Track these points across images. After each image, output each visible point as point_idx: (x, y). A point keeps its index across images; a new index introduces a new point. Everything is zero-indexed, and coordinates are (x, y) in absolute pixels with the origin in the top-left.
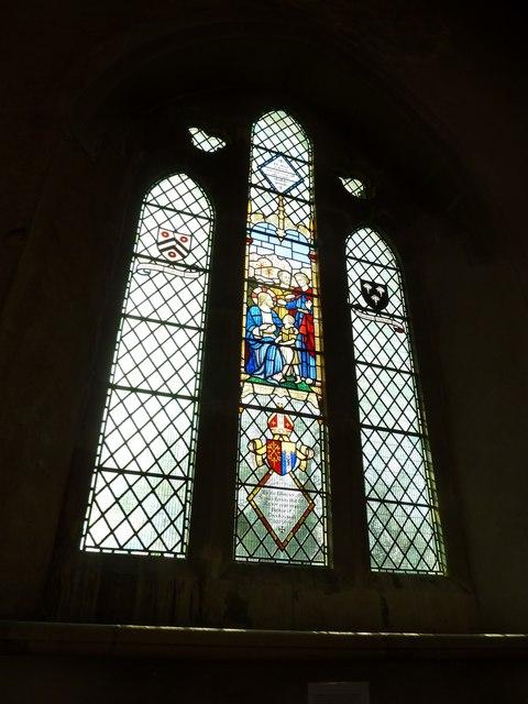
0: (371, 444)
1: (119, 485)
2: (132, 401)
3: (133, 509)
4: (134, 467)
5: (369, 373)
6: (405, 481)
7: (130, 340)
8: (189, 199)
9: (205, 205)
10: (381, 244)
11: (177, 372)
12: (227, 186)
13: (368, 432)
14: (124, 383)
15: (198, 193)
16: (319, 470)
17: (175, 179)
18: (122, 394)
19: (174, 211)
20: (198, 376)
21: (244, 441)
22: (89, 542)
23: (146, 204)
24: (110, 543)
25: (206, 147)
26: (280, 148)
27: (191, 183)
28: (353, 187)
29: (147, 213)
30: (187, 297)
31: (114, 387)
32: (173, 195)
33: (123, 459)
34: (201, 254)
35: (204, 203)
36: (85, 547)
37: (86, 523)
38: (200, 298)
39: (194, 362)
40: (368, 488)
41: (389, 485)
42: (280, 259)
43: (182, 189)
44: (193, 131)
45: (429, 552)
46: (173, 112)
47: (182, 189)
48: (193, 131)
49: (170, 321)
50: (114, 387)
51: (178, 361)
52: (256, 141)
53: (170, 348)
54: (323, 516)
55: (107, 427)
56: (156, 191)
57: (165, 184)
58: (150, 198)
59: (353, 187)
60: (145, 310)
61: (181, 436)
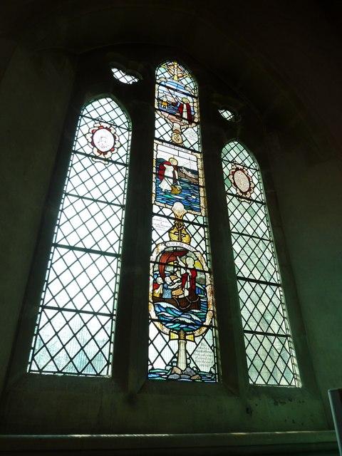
0: (245, 291)
1: (59, 321)
2: (70, 257)
3: (72, 329)
4: (70, 306)
5: (240, 240)
6: (269, 318)
7: (69, 212)
8: (113, 115)
9: (125, 120)
10: (245, 152)
11: (101, 273)
12: (140, 106)
13: (249, 336)
14: (64, 242)
15: (119, 111)
16: (203, 242)
17: (103, 101)
18: (63, 251)
19: (102, 126)
20: (116, 296)
21: (151, 350)
22: (34, 367)
23: (82, 116)
24: (51, 368)
25: (123, 80)
26: (174, 83)
27: (114, 104)
28: (227, 115)
29: (82, 122)
30: (114, 182)
31: (56, 245)
32: (101, 111)
33: (62, 300)
34: (123, 154)
35: (124, 118)
36: (30, 370)
37: (32, 351)
38: (118, 230)
39: (112, 284)
40: (244, 323)
41: (238, 218)
42: (178, 149)
43: (108, 108)
44: (114, 70)
45: (275, 297)
46: (100, 55)
47: (108, 108)
48: (114, 70)
49: (94, 248)
50: (56, 245)
51: (99, 283)
52: (157, 135)
53: (93, 272)
54: (213, 345)
55: (51, 276)
56: (89, 108)
57: (96, 104)
58: (85, 112)
59: (227, 115)
60: (73, 241)
61: (103, 327)
